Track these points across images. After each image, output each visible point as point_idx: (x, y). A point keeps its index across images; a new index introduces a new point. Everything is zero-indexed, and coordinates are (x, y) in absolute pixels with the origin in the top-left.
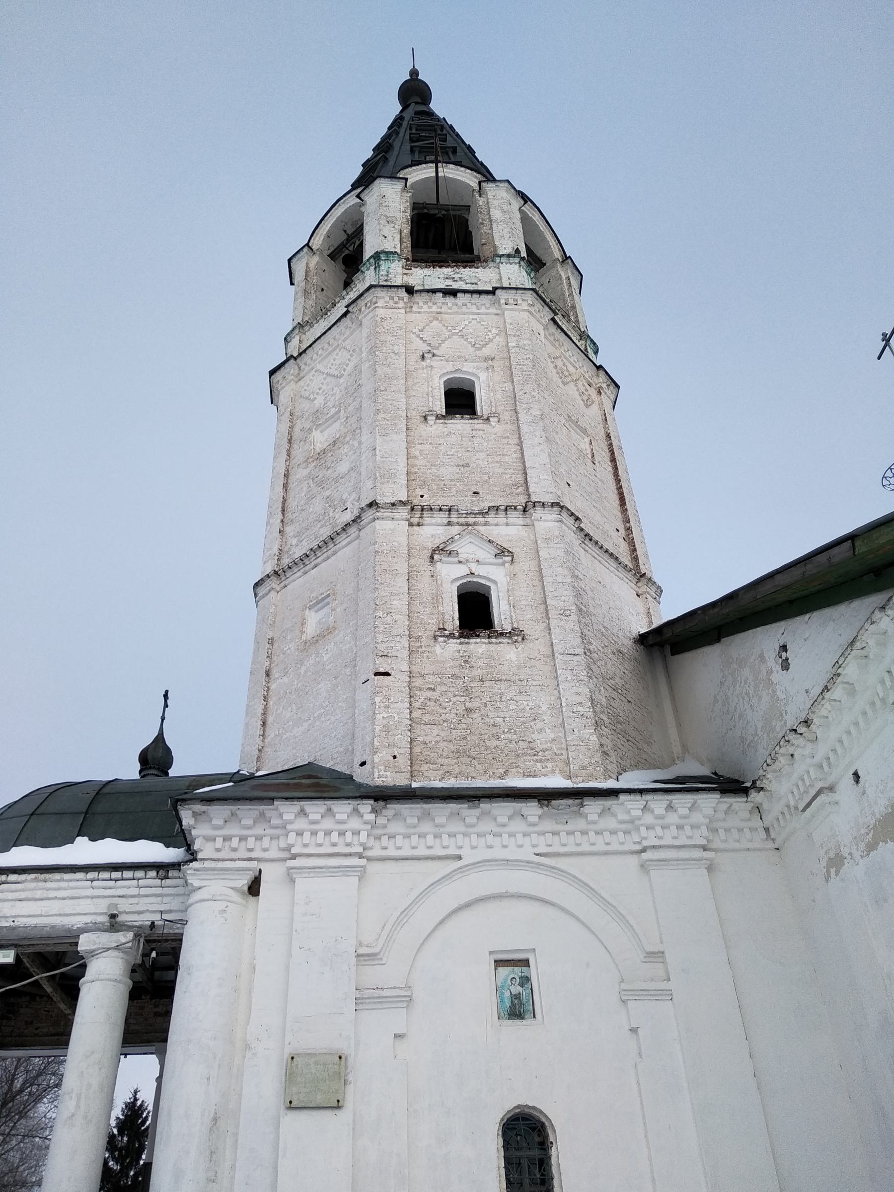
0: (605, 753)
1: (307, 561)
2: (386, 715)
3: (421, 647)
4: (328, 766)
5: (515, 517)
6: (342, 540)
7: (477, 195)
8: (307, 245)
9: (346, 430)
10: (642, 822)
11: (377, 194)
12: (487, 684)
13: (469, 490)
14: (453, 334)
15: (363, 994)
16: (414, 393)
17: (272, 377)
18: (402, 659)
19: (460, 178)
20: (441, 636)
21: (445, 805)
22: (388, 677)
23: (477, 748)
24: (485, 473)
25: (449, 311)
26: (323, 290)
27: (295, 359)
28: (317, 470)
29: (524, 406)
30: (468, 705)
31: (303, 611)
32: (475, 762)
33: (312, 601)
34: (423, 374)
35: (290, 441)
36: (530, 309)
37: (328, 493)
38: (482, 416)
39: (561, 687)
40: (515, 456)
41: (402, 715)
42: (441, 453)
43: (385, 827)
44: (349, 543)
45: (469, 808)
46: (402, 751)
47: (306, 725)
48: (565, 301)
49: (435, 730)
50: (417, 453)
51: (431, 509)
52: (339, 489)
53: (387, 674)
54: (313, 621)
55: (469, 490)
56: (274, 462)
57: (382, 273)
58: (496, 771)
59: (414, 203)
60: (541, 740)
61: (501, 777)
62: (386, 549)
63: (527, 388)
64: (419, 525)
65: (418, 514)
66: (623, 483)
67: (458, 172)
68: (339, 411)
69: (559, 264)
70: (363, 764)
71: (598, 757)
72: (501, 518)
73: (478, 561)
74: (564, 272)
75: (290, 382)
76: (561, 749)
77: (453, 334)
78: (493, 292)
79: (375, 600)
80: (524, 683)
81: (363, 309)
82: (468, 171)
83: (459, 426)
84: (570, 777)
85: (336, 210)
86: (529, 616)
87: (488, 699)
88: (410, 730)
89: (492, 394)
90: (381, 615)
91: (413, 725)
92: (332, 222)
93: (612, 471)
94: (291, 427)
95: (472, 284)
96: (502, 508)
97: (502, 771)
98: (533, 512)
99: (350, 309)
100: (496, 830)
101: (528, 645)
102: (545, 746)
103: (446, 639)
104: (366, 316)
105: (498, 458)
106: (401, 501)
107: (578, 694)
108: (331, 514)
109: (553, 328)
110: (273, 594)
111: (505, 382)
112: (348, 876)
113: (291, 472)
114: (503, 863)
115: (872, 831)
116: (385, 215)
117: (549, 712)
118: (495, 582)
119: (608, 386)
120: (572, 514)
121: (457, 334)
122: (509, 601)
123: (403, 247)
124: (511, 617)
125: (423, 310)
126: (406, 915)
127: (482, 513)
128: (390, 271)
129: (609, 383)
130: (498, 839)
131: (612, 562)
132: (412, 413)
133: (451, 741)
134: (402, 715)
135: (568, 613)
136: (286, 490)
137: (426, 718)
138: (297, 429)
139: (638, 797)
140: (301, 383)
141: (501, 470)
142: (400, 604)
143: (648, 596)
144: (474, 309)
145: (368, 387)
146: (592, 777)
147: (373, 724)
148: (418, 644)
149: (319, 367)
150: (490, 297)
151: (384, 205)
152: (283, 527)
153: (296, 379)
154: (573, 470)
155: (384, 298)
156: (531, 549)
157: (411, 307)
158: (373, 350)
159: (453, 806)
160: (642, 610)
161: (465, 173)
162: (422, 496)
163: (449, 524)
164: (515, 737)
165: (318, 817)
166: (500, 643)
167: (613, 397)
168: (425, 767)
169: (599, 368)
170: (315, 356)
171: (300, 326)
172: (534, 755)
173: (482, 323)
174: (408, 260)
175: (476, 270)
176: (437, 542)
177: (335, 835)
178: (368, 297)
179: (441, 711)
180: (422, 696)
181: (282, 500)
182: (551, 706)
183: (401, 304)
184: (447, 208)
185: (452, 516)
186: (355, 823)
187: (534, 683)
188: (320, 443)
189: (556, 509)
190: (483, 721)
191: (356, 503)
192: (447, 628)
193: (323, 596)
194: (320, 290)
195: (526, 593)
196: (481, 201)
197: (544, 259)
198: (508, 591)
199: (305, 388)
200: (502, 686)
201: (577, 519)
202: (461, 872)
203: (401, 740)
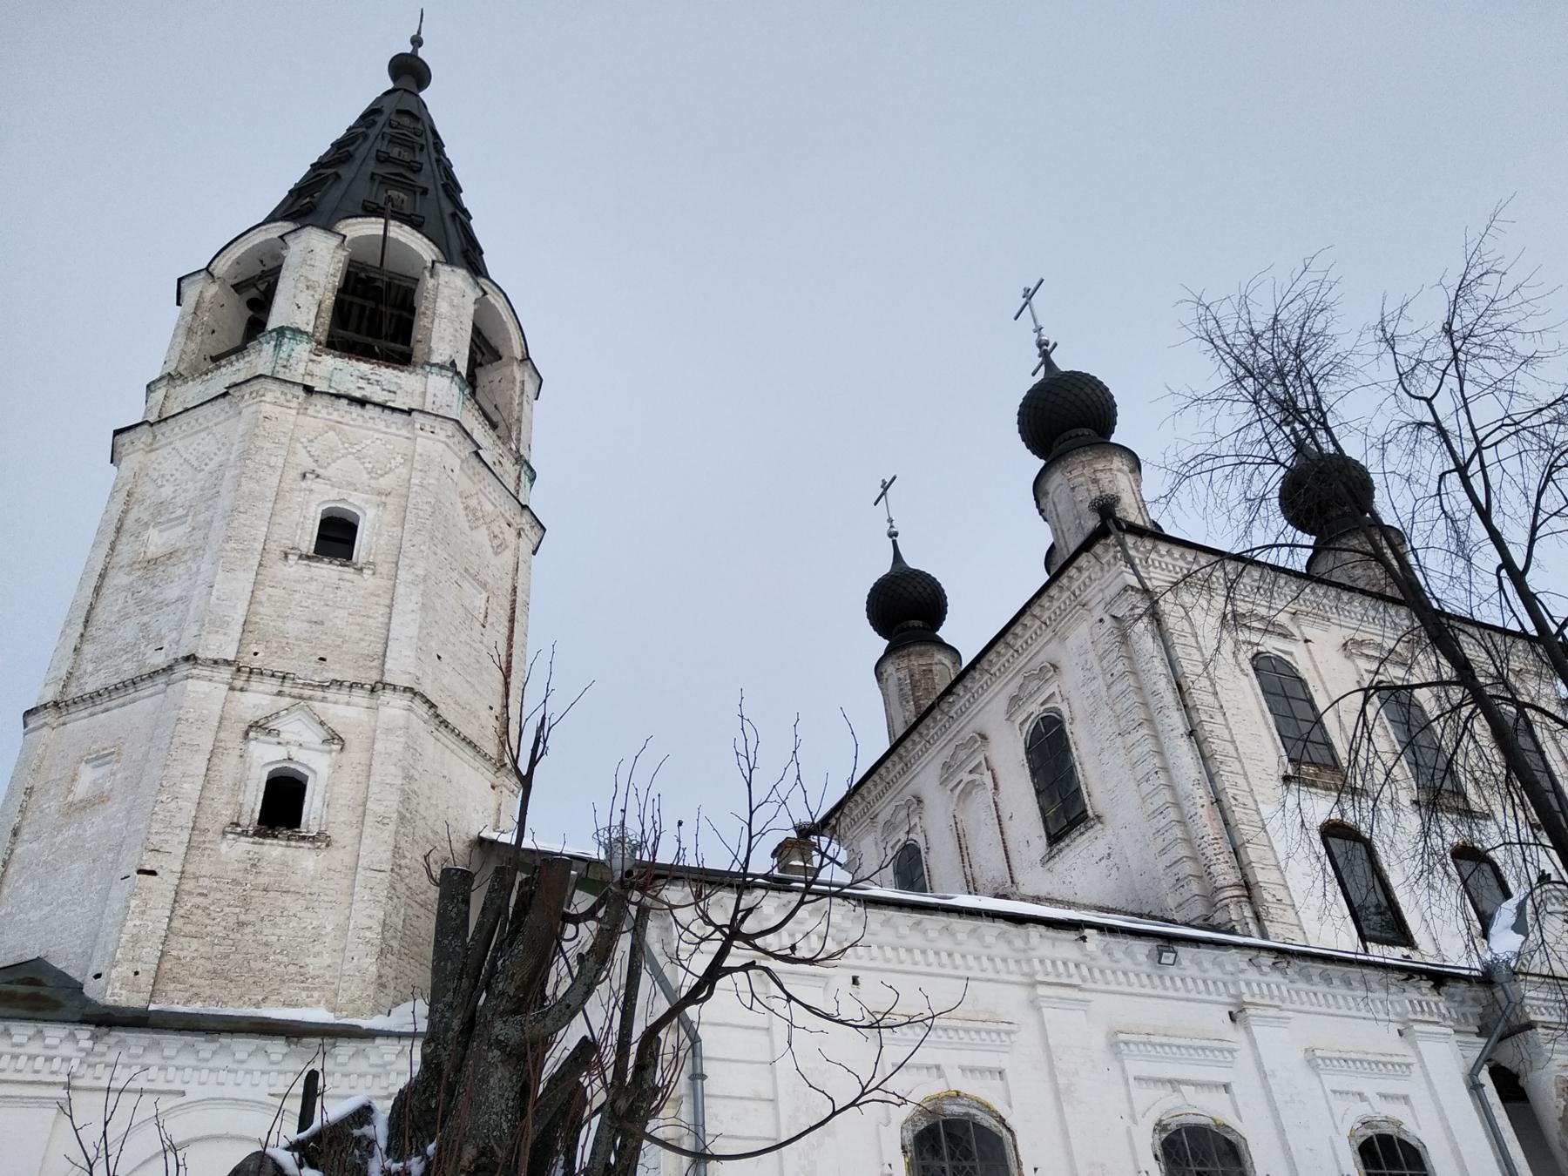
0: (383, 986)
1: (98, 700)
2: (138, 923)
3: (204, 842)
4: (59, 967)
5: (360, 697)
6: (147, 689)
7: (428, 275)
8: (207, 269)
9: (188, 545)
10: (393, 1067)
11: (304, 244)
12: (271, 894)
13: (315, 654)
14: (350, 453)
16: (280, 521)
17: (117, 437)
18: (176, 856)
19: (413, 246)
20: (231, 833)
21: (179, 1037)
22: (154, 877)
23: (238, 970)
24: (339, 637)
25: (352, 423)
26: (213, 332)
27: (152, 425)
28: (141, 582)
29: (408, 561)
30: (242, 918)
31: (77, 763)
32: (231, 985)
33: (90, 754)
34: (299, 498)
35: (118, 530)
36: (448, 441)
37: (146, 619)
38: (355, 564)
39: (353, 907)
40: (381, 619)
41: (157, 925)
42: (294, 603)
43: (103, 1054)
44: (152, 695)
45: (206, 1041)
46: (146, 967)
47: (46, 909)
48: (511, 412)
49: (195, 944)
50: (264, 598)
51: (262, 673)
52: (160, 618)
53: (153, 873)
54: (88, 778)
55: (315, 654)
56: (92, 551)
57: (282, 355)
58: (253, 997)
59: (351, 260)
60: (314, 965)
61: (257, 1005)
62: (192, 716)
63: (418, 539)
64: (242, 690)
65: (244, 676)
66: (515, 651)
67: (412, 238)
68: (187, 515)
69: (515, 363)
70: (98, 976)
71: (371, 991)
72: (343, 695)
73: (301, 745)
74: (518, 373)
75: (138, 450)
76: (335, 977)
77: (350, 453)
78: (409, 412)
79: (161, 779)
80: (315, 897)
81: (247, 397)
82: (425, 240)
83: (324, 572)
84: (334, 1010)
85: (255, 234)
86: (342, 819)
87: (267, 913)
88: (163, 944)
89: (375, 539)
90: (164, 799)
91: (170, 935)
92: (246, 248)
93: (507, 633)
94: (125, 512)
95: (390, 391)
96: (347, 684)
97: (260, 998)
99: (231, 391)
100: (233, 1066)
101: (333, 851)
102: (317, 973)
103: (236, 836)
104: (247, 406)
105: (360, 620)
106: (225, 660)
107: (370, 917)
108: (142, 648)
109: (474, 461)
110: (45, 730)
111: (394, 526)
113: (111, 573)
116: (306, 278)
117: (332, 935)
118: (315, 772)
119: (532, 527)
120: (427, 701)
121: (353, 454)
122: (324, 798)
123: (318, 323)
124: (322, 817)
125: (320, 415)
127: (322, 687)
128: (293, 355)
129: (533, 524)
130: (232, 1076)
131: (469, 751)
132: (272, 546)
133: (209, 958)
134: (157, 925)
135: (386, 821)
136: (97, 595)
137: (189, 929)
138: (132, 515)
139: (395, 1041)
140: (153, 456)
141: (360, 635)
142: (191, 788)
143: (504, 789)
144: (382, 425)
145: (224, 503)
146: (358, 1012)
147: (121, 931)
148: (202, 839)
149: (178, 444)
150: (405, 416)
151: (309, 262)
152: (81, 643)
153: (147, 449)
154: (451, 638)
155: (274, 391)
156: (367, 738)
157: (307, 409)
158: (245, 456)
160: (493, 805)
161: (421, 240)
162: (256, 654)
163: (280, 693)
164: (286, 959)
165: (24, 1039)
167: (535, 540)
168: (172, 986)
169: (525, 507)
170: (177, 429)
171: (170, 377)
172: (303, 982)
173: (388, 446)
174: (319, 343)
175: (400, 374)
176: (258, 715)
177: (40, 1060)
178: (256, 385)
179: (208, 922)
180: (189, 902)
181: (87, 607)
182: (337, 927)
183: (294, 404)
184: (393, 275)
185: (285, 684)
186: (67, 1049)
187: (326, 898)
188: (156, 546)
189: (409, 695)
190: (254, 938)
191: (173, 645)
192: (241, 823)
193: (105, 752)
194: (210, 331)
195: (346, 790)
196: (430, 283)
197: (502, 351)
198: (327, 786)
199: (155, 465)
200: (288, 899)
201: (433, 706)
203: (150, 953)
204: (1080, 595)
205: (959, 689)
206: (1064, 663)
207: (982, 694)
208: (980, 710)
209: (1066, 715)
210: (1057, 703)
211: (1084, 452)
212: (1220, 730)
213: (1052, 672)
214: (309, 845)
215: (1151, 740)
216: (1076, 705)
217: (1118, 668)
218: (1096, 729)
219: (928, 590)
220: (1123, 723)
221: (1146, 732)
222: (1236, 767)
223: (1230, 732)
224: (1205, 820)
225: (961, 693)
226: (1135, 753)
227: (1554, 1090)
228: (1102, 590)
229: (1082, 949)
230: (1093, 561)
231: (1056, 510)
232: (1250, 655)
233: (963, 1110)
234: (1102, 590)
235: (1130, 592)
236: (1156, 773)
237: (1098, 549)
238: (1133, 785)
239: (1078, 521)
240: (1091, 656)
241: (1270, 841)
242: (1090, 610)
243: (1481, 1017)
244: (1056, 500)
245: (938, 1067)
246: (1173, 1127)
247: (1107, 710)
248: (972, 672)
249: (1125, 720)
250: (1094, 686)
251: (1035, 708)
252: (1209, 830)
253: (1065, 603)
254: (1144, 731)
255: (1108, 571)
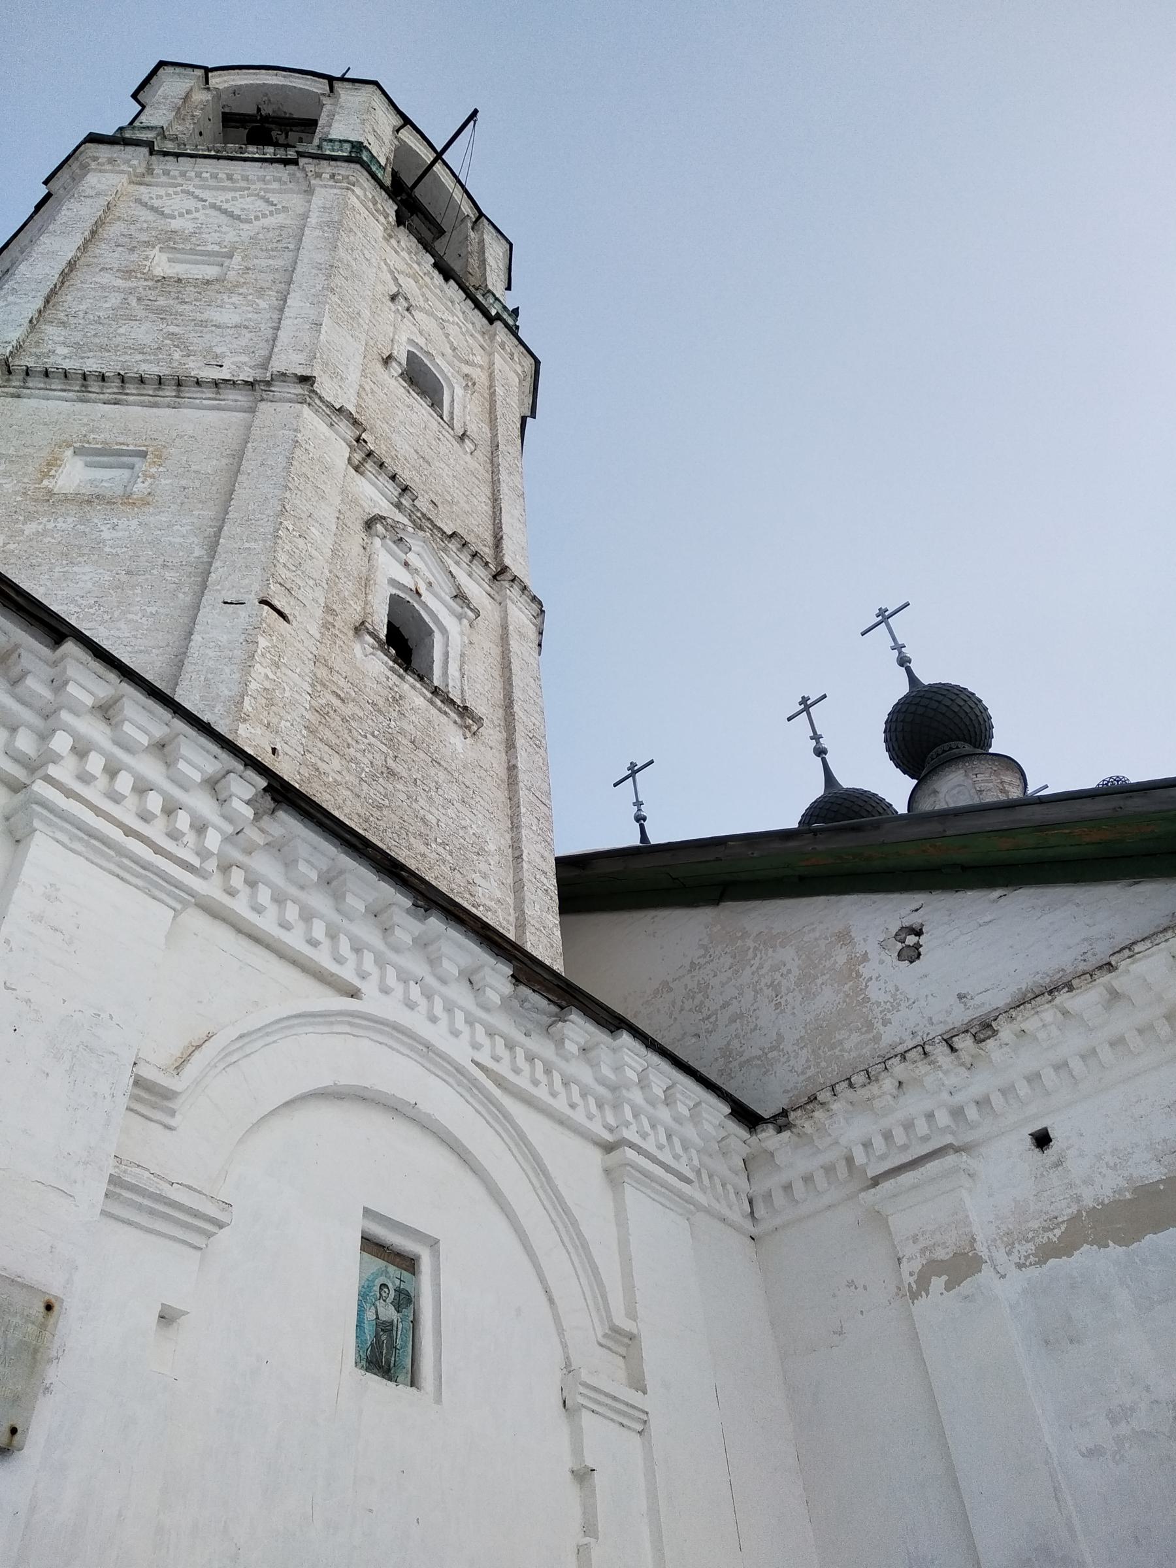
8: (207, 70)
15: (125, 1172)
45: (408, 911)
98: (507, 586)
102: (488, 903)
112: (154, 898)
114: (421, 1047)
115: (1063, 1228)
126: (241, 1048)
159: (387, 891)
166: (445, 713)
202: (350, 1024)
208: (143, 1116)
214: (454, 716)
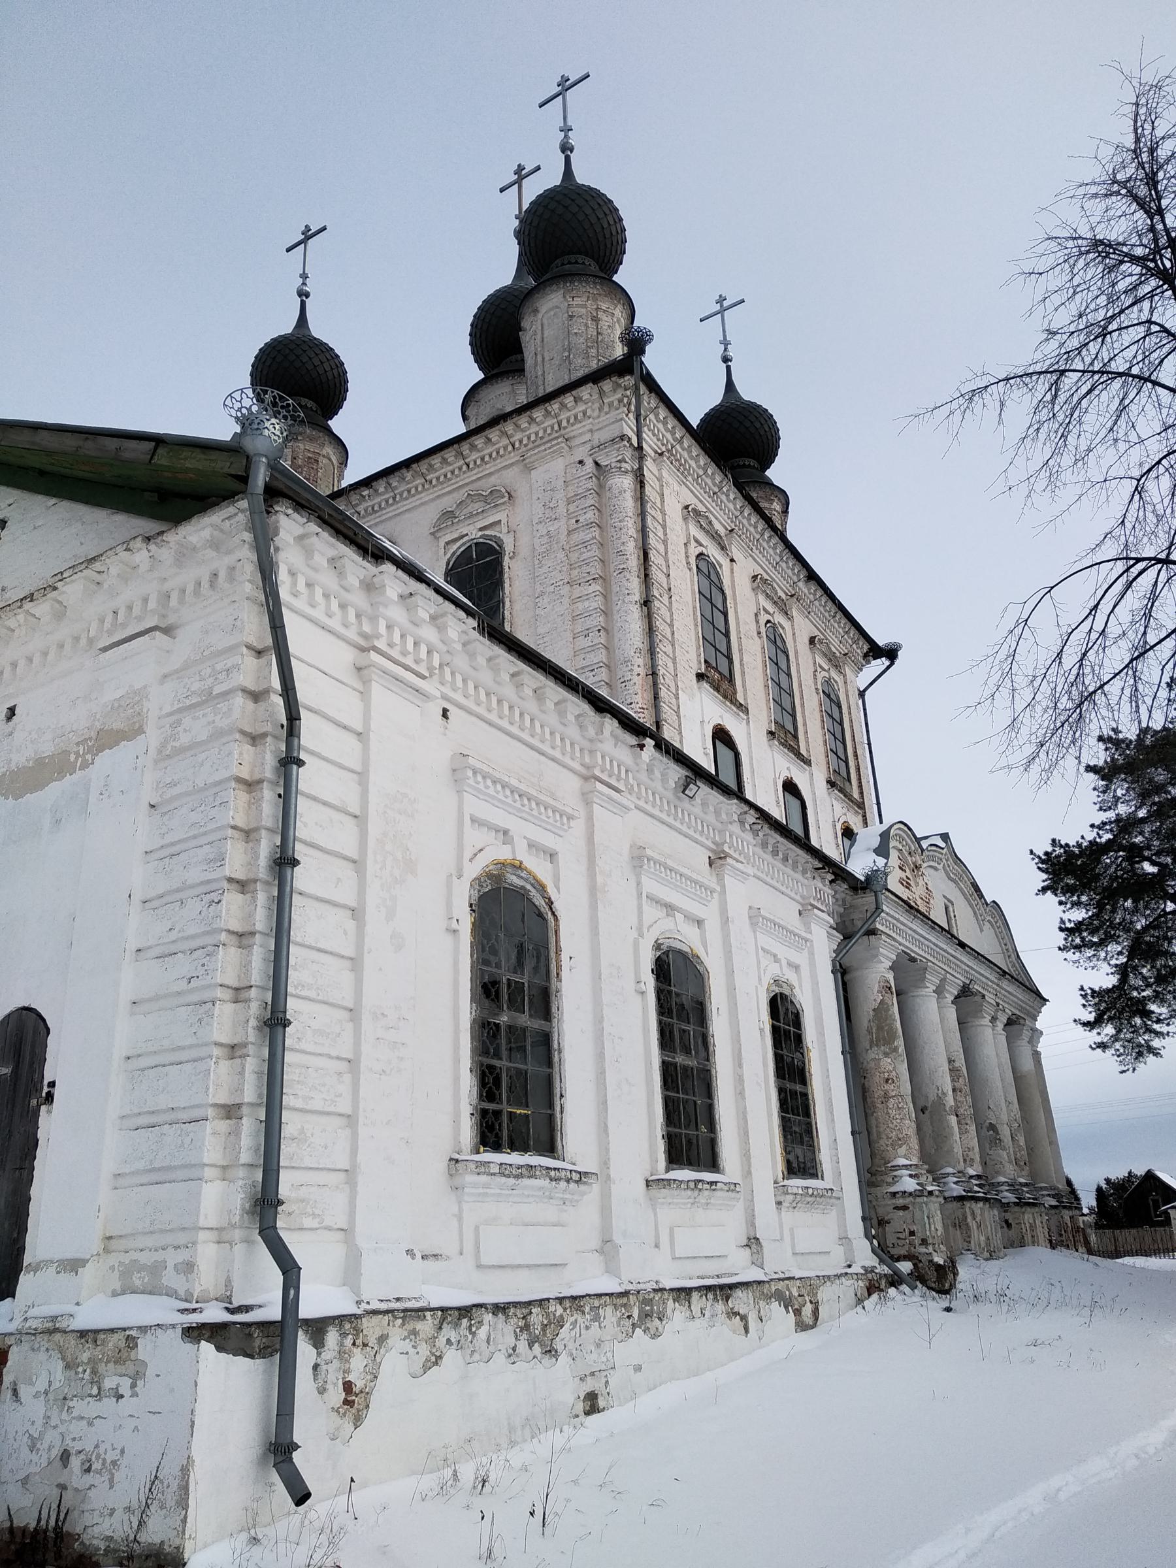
204: (565, 428)
205: (381, 486)
206: (521, 491)
207: (406, 499)
209: (508, 547)
210: (501, 533)
211: (594, 283)
212: (664, 611)
213: (506, 499)
215: (600, 598)
216: (524, 540)
217: (588, 516)
218: (542, 571)
219: (335, 372)
220: (575, 572)
221: (598, 588)
222: (669, 649)
223: (671, 615)
224: (638, 688)
225: (381, 490)
226: (580, 606)
227: (877, 986)
228: (591, 431)
229: (637, 758)
230: (596, 396)
231: (543, 334)
232: (697, 553)
233: (521, 883)
234: (591, 431)
235: (626, 443)
236: (599, 631)
237: (607, 385)
238: (569, 636)
239: (566, 354)
240: (560, 495)
241: (680, 725)
242: (570, 448)
243: (841, 915)
244: (545, 321)
245: (506, 832)
246: (664, 948)
247: (561, 555)
248: (404, 471)
249: (578, 570)
250: (553, 527)
251: (472, 531)
252: (639, 698)
253: (545, 431)
254: (596, 587)
255: (607, 413)
